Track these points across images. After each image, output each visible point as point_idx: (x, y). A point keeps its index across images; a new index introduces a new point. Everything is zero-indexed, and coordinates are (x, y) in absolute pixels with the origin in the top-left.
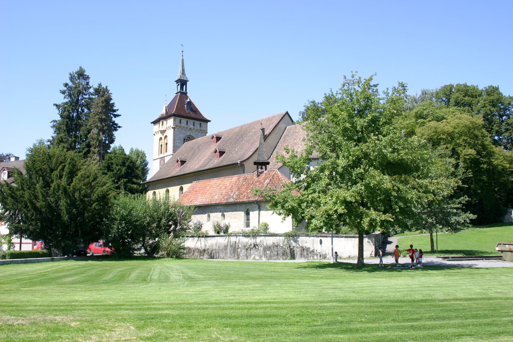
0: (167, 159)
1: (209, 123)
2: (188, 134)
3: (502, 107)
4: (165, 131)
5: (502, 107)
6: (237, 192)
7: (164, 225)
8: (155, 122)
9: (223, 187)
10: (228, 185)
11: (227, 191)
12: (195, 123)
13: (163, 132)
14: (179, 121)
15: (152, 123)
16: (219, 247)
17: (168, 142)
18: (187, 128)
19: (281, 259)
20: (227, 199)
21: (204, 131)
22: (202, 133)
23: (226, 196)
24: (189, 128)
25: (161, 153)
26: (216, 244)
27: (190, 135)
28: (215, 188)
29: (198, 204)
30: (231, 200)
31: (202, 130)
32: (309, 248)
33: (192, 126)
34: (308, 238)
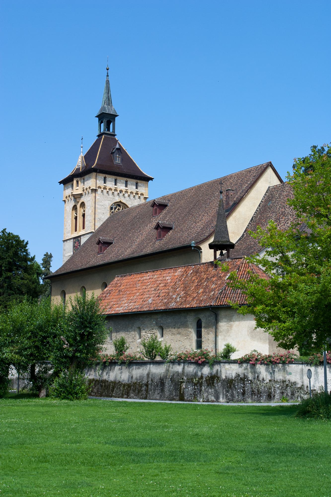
0: (83, 240)
1: (150, 181)
3: (270, 223)
4: (81, 195)
5: (270, 223)
6: (183, 293)
7: (297, 211)
8: (67, 182)
9: (162, 285)
10: (169, 281)
11: (167, 291)
13: (77, 197)
15: (60, 183)
16: (152, 380)
17: (86, 213)
19: (249, 400)
20: (167, 303)
23: (165, 299)
25: (76, 231)
26: (148, 375)
27: (120, 202)
28: (149, 286)
29: (123, 311)
30: (173, 305)
32: (295, 383)
34: (276, 185)
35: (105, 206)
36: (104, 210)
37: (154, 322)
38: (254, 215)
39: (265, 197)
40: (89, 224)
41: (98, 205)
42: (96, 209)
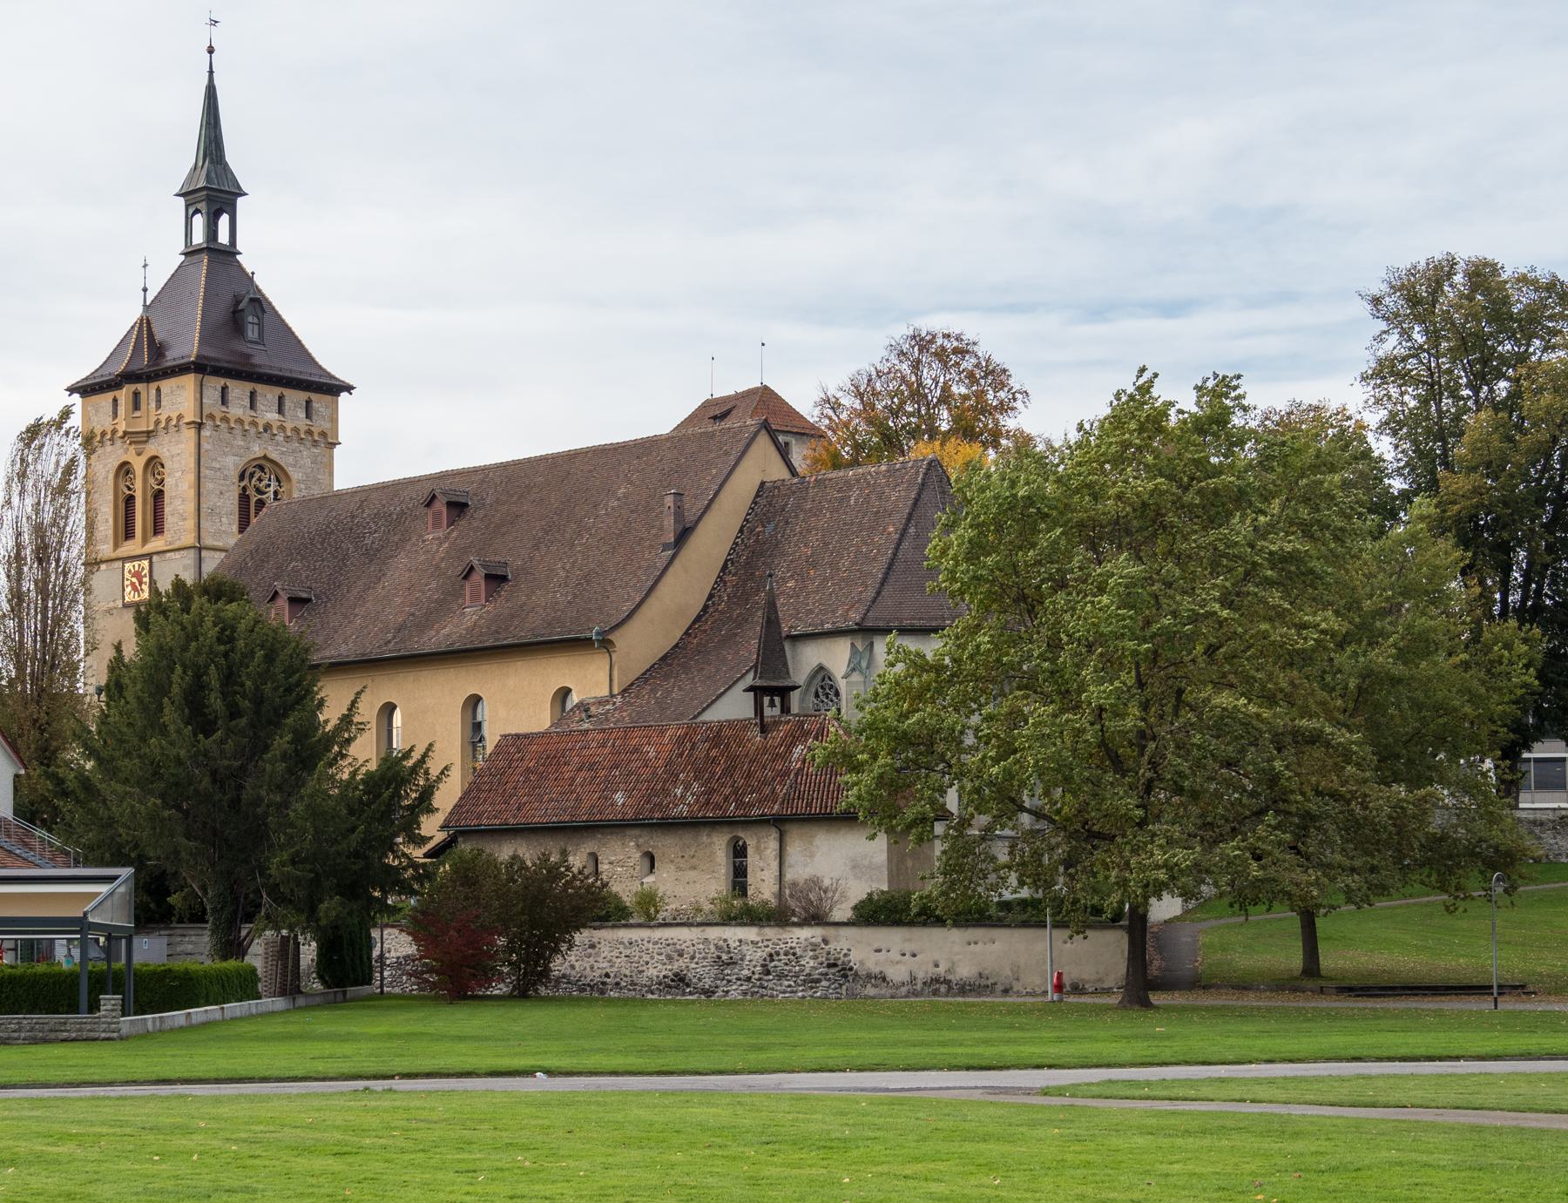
1: (344, 395)
2: (259, 454)
12: (288, 404)
14: (218, 394)
18: (254, 424)
21: (323, 434)
22: (315, 443)
24: (261, 423)
25: (129, 534)
27: (265, 457)
31: (316, 430)
33: (272, 416)
35: (226, 472)
36: (222, 482)
37: (632, 844)
38: (729, 554)
39: (753, 509)
40: (180, 523)
41: (207, 468)
42: (202, 480)
